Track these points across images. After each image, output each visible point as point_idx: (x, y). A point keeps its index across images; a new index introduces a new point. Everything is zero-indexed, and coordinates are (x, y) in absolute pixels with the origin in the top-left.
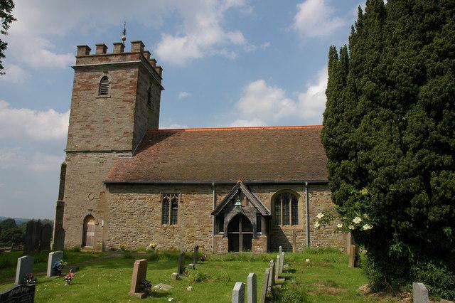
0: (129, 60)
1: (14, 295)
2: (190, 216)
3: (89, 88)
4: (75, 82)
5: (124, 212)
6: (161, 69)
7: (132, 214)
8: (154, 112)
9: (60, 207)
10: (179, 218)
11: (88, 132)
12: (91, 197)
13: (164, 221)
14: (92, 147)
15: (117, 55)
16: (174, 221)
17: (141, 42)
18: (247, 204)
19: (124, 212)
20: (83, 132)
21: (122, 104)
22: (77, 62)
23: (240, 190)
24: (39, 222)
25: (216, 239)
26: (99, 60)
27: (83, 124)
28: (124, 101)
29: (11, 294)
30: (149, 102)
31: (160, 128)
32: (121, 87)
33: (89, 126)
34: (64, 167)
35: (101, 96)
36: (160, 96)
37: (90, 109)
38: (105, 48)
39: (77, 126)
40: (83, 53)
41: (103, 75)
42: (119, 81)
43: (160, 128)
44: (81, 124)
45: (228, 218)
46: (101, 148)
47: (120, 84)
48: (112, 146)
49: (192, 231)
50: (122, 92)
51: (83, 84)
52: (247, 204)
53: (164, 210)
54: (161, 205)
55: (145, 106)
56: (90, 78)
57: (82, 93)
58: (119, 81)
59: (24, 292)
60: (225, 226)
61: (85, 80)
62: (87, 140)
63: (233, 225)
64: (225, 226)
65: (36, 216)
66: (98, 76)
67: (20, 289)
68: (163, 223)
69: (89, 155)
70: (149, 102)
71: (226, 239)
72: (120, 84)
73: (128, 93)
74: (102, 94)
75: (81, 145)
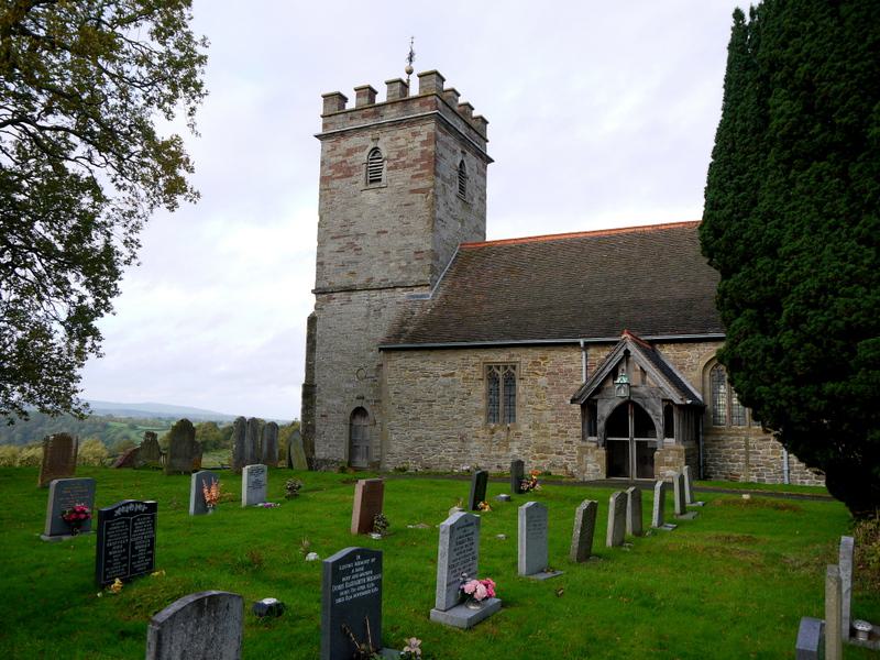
0: (417, 110)
1: (124, 514)
2: (539, 406)
3: (348, 172)
4: (323, 163)
5: (417, 401)
6: (485, 122)
7: (431, 403)
8: (475, 208)
9: (309, 392)
10: (519, 412)
11: (350, 256)
12: (362, 373)
13: (492, 415)
14: (359, 281)
15: (395, 102)
16: (511, 416)
17: (436, 73)
18: (644, 382)
19: (417, 401)
20: (342, 257)
21: (410, 198)
22: (325, 126)
23: (627, 353)
24: (254, 421)
25: (583, 451)
26: (364, 116)
27: (341, 240)
28: (413, 191)
29: (118, 512)
30: (462, 189)
31: (489, 238)
32: (405, 166)
33: (351, 245)
34: (312, 321)
35: (373, 185)
36: (484, 176)
37: (353, 212)
38: (372, 92)
39: (333, 246)
40: (334, 108)
41: (372, 145)
42: (400, 154)
43: (489, 238)
44: (337, 241)
45: (605, 409)
46: (373, 284)
47: (402, 159)
48: (399, 277)
49: (545, 435)
50: (409, 172)
51: (337, 167)
52: (644, 382)
53: (492, 394)
54: (482, 387)
55: (453, 198)
56: (348, 155)
57: (336, 183)
58: (400, 154)
59: (139, 512)
60: (601, 425)
61: (341, 158)
62: (351, 269)
63: (617, 422)
64: (601, 425)
65: (291, 419)
66: (363, 148)
67: (132, 506)
68: (488, 421)
69: (354, 296)
70: (462, 189)
71: (602, 452)
72: (402, 159)
73: (417, 176)
74: (371, 181)
75: (341, 279)
